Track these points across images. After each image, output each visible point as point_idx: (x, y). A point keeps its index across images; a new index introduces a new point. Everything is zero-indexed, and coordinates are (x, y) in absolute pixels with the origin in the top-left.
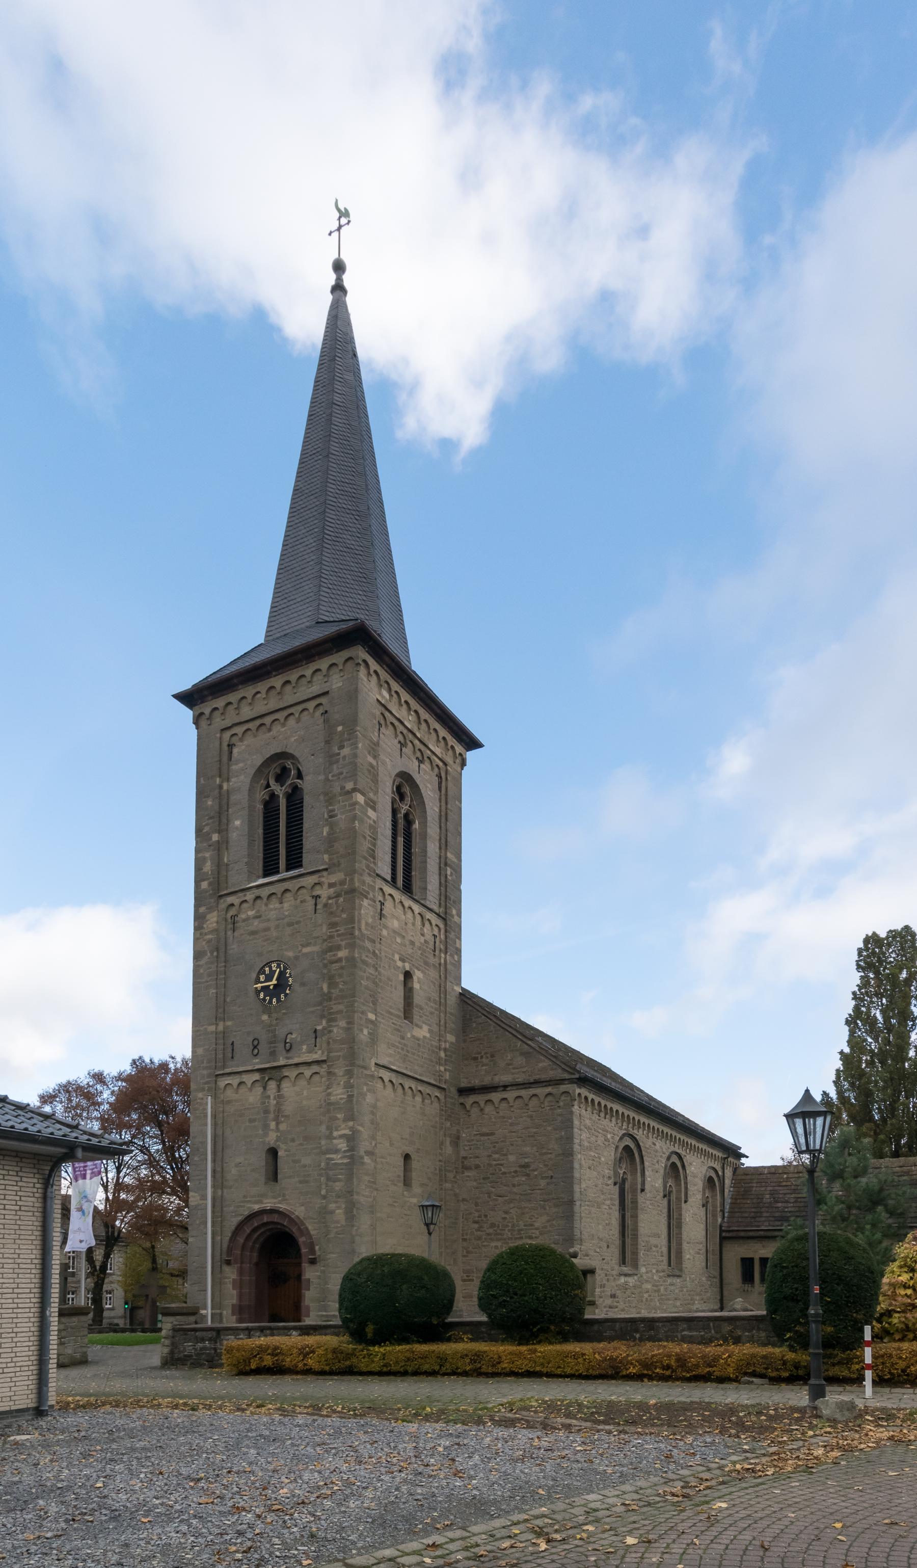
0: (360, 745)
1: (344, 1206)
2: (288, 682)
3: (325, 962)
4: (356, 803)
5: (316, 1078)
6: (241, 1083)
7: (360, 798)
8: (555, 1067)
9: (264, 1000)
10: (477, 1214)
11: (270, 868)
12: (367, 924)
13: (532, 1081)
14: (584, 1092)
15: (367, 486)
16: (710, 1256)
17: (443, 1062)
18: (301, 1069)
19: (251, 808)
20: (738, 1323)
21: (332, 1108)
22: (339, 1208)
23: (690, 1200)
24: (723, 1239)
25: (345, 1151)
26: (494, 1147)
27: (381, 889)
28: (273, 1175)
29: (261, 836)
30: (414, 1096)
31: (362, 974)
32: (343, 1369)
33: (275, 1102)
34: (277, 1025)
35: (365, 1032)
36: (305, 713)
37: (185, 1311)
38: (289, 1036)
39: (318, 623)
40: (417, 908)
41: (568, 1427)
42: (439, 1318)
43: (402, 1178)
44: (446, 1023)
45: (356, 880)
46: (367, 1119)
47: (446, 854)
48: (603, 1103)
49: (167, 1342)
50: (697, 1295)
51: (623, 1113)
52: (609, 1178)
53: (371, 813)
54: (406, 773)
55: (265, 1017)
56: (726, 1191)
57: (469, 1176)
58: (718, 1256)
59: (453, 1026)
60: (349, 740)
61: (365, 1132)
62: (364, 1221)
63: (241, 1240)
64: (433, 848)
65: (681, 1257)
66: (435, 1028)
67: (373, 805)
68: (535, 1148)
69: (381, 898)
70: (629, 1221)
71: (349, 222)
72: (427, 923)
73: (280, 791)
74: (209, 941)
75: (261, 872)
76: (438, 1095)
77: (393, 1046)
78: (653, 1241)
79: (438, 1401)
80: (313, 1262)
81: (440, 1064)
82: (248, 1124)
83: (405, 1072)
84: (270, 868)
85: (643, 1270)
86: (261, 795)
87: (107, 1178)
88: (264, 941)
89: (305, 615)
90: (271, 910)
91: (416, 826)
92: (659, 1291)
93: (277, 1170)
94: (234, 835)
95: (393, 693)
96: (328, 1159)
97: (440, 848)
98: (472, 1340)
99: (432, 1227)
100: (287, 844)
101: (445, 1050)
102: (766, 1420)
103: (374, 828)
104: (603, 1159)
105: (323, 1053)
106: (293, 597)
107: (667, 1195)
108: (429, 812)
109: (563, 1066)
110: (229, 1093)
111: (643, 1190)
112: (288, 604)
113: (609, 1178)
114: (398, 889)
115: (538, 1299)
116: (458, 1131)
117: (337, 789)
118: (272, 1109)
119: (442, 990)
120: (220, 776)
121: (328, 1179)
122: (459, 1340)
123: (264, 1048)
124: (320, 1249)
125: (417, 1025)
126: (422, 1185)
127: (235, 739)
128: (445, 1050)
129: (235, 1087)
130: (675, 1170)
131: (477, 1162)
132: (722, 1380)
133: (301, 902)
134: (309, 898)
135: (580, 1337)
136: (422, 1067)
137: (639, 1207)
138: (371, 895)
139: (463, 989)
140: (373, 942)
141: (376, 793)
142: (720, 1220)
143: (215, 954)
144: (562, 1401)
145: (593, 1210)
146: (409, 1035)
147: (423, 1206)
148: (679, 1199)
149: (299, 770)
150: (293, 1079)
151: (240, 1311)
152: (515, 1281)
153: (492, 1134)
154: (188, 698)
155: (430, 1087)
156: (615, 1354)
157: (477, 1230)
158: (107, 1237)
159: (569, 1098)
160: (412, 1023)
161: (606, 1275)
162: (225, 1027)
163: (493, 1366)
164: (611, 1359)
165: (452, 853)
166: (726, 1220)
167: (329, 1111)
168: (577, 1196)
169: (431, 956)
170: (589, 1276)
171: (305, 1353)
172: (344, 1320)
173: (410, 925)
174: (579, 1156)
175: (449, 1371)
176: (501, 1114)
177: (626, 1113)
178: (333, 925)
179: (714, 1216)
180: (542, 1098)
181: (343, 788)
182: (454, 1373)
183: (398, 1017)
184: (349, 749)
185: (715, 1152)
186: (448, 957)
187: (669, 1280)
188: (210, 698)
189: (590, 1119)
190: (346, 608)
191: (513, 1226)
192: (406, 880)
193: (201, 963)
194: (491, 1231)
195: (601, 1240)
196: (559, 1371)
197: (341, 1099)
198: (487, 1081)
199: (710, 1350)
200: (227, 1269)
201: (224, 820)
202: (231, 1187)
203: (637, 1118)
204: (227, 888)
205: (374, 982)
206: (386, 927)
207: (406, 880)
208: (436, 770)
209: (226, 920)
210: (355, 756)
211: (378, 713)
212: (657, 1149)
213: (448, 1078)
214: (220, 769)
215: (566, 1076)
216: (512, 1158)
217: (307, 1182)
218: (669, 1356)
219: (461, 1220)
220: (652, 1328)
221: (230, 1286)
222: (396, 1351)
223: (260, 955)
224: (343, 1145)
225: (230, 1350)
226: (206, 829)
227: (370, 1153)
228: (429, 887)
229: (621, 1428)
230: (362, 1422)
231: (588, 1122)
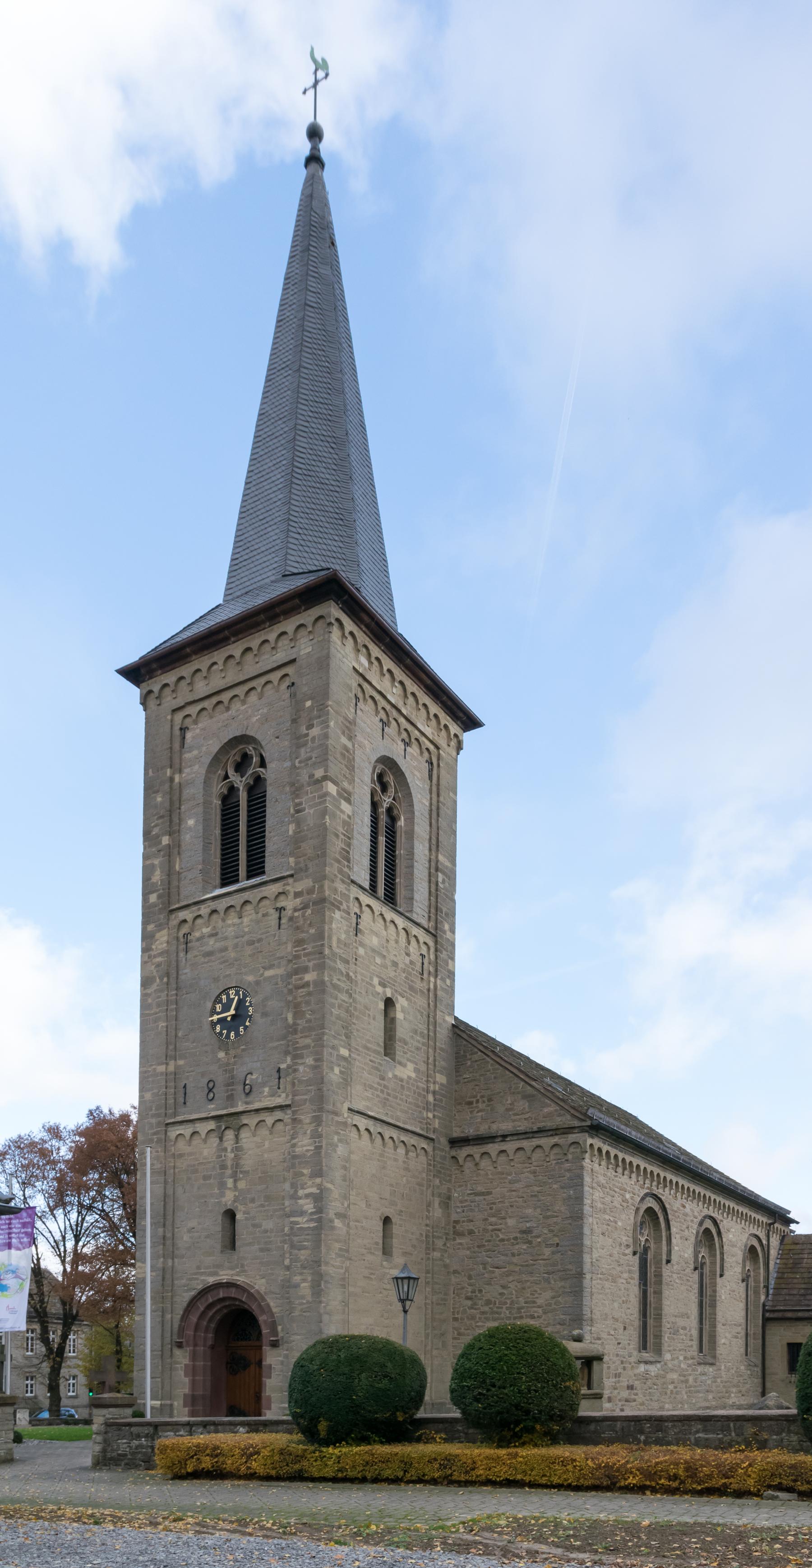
0: (332, 724)
1: (310, 1278)
2: (249, 649)
3: (290, 987)
4: (327, 794)
5: (280, 1126)
6: (195, 1133)
7: (332, 788)
8: (562, 1112)
9: (221, 1034)
10: (470, 1289)
11: (228, 876)
12: (339, 940)
13: (535, 1129)
14: (597, 1143)
15: (345, 405)
16: (751, 1341)
17: (432, 1107)
18: (263, 1116)
19: (206, 804)
20: (764, 1424)
21: (297, 1161)
22: (304, 1280)
23: (726, 1273)
24: (766, 1321)
25: (312, 1214)
26: (491, 1209)
27: (357, 899)
28: (231, 1243)
29: (219, 837)
30: (396, 1148)
31: (333, 1001)
32: (295, 1475)
33: (233, 1155)
34: (235, 1063)
35: (337, 1070)
36: (269, 686)
37: (119, 1402)
38: (249, 1076)
39: (284, 576)
40: (401, 922)
41: (533, 1554)
42: (405, 1413)
43: (381, 1246)
44: (435, 1060)
45: (326, 887)
46: (338, 1174)
47: (437, 857)
48: (621, 1156)
49: (99, 1438)
50: (734, 1386)
51: (645, 1169)
52: (628, 1246)
53: (344, 805)
54: (389, 758)
55: (221, 1055)
56: (772, 1263)
57: (461, 1244)
58: (760, 1341)
59: (443, 1063)
60: (319, 717)
61: (335, 1191)
62: (334, 1298)
63: (194, 1319)
64: (421, 850)
65: (715, 1343)
66: (423, 1067)
67: (347, 797)
68: (539, 1210)
69: (357, 911)
70: (651, 1298)
71: (327, 75)
72: (413, 940)
73: (240, 782)
74: (158, 965)
75: (218, 881)
76: (425, 1147)
77: (371, 1087)
78: (681, 1322)
79: (390, 1516)
80: (275, 1345)
81: (428, 1110)
82: (202, 1182)
83: (384, 1118)
84: (228, 876)
85: (668, 1356)
86: (218, 788)
87: (65, 1247)
88: (221, 963)
89: (270, 568)
90: (229, 926)
91: (401, 823)
92: (687, 1381)
93: (234, 1236)
94: (187, 838)
95: (373, 660)
96: (292, 1222)
97: (430, 850)
98: (446, 1440)
99: (408, 1303)
100: (248, 846)
101: (434, 1093)
102: (780, 1550)
103: (348, 825)
104: (620, 1224)
105: (287, 1096)
106: (256, 547)
107: (699, 1267)
108: (417, 807)
109: (572, 1111)
110: (182, 1146)
111: (668, 1261)
112: (251, 555)
113: (628, 1246)
114: (378, 898)
115: (520, 1392)
116: (449, 1190)
117: (304, 777)
118: (229, 1163)
119: (431, 1021)
120: (171, 767)
121: (292, 1246)
122: (430, 1440)
123: (220, 1091)
124: (282, 1330)
125: (400, 1063)
126: (405, 1254)
127: (188, 720)
128: (434, 1093)
129: (188, 1137)
130: (709, 1237)
131: (471, 1226)
132: (740, 1494)
133: (264, 915)
134: (272, 911)
135: (573, 1439)
136: (406, 1112)
137: (664, 1281)
138: (344, 906)
139: (456, 1018)
140: (347, 962)
141: (352, 781)
142: (763, 1298)
143: (165, 980)
144: (537, 1519)
145: (607, 1284)
146: (390, 1075)
147: (397, 1278)
148: (713, 1273)
149: (262, 757)
150: (253, 1128)
151: (192, 1401)
152: (493, 1369)
153: (489, 1193)
154: (134, 673)
155: (416, 1138)
156: (611, 1461)
157: (471, 1308)
158: (65, 1314)
159: (578, 1150)
160: (394, 1060)
161: (622, 1362)
162: (177, 1067)
163: (467, 1472)
164: (607, 1466)
165: (445, 856)
166: (770, 1297)
167: (293, 1166)
168: (587, 1267)
169: (418, 981)
170: (595, 1363)
171: (250, 1453)
172: (295, 1415)
173: (392, 943)
174: (590, 1220)
175: (414, 1478)
176: (499, 1169)
177: (649, 1168)
178: (299, 942)
179: (757, 1293)
180: (547, 1149)
181: (312, 776)
182: (420, 1481)
183: (375, 1051)
184: (319, 728)
185: (758, 1217)
186: (439, 982)
187: (700, 1369)
188: (160, 672)
189: (605, 1175)
190: (318, 557)
191: (512, 1303)
192: (388, 885)
193: (149, 991)
194: (486, 1309)
195: (617, 1320)
196: (544, 1481)
197: (307, 1151)
198: (483, 1130)
199: (728, 1457)
200: (177, 1352)
201: (176, 820)
202: (182, 1257)
203: (662, 1175)
204: (179, 901)
205: (347, 1011)
206: (362, 944)
207: (388, 885)
208: (426, 754)
209: (178, 939)
210: (326, 736)
211: (355, 685)
212: (687, 1212)
213: (437, 1126)
214: (171, 758)
215: (576, 1123)
216: (511, 1222)
217: (268, 1250)
218: (677, 1464)
219: (452, 1296)
220: (659, 1429)
221: (182, 1373)
222: (352, 1453)
223: (216, 980)
224: (309, 1206)
225: (164, 1450)
226: (155, 831)
227: (339, 1215)
228: (417, 896)
229: (597, 1558)
230: (284, 1543)
231: (602, 1179)
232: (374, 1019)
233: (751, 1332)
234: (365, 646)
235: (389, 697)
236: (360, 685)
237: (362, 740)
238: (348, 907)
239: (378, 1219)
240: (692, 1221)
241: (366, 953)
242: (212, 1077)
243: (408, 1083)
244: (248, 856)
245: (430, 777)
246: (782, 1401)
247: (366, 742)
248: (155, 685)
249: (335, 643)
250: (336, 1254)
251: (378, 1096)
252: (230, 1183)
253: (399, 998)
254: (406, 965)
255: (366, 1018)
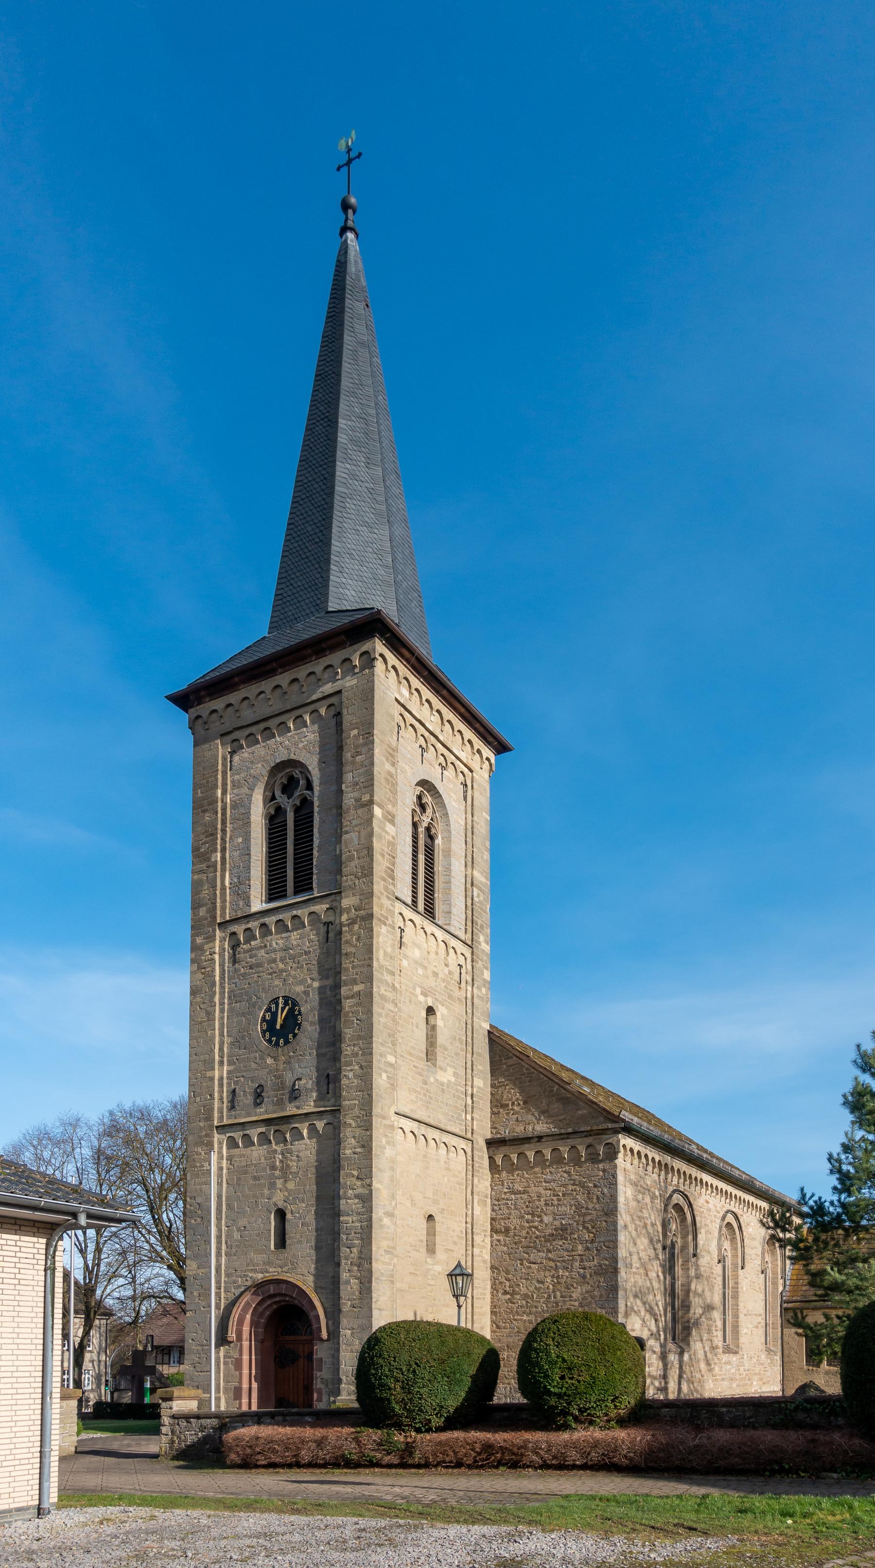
2: (295, 680)
12: (385, 952)
16: (770, 1331)
23: (747, 1265)
27: (401, 914)
31: (380, 1011)
35: (384, 1076)
53: (389, 827)
72: (451, 951)
73: (288, 805)
77: (415, 1091)
91: (439, 841)
97: (466, 866)
100: (295, 864)
103: (392, 845)
108: (453, 826)
123: (269, 1095)
138: (390, 922)
141: (394, 804)
166: (787, 1288)
173: (433, 955)
179: (775, 1284)
186: (475, 990)
188: (208, 699)
206: (406, 957)
228: (454, 910)
232: (417, 1027)
233: (770, 1321)
234: (406, 679)
235: (427, 725)
236: (401, 715)
237: (404, 765)
238: (393, 922)
239: (422, 1217)
240: (715, 1216)
241: (409, 964)
242: (263, 1082)
243: (448, 1086)
244: (295, 873)
245: (465, 798)
246: (828, 1380)
247: (407, 767)
248: (204, 709)
249: (379, 676)
250: (385, 1251)
251: (421, 1100)
252: (279, 1183)
253: (440, 1006)
254: (445, 975)
255: (410, 1026)
